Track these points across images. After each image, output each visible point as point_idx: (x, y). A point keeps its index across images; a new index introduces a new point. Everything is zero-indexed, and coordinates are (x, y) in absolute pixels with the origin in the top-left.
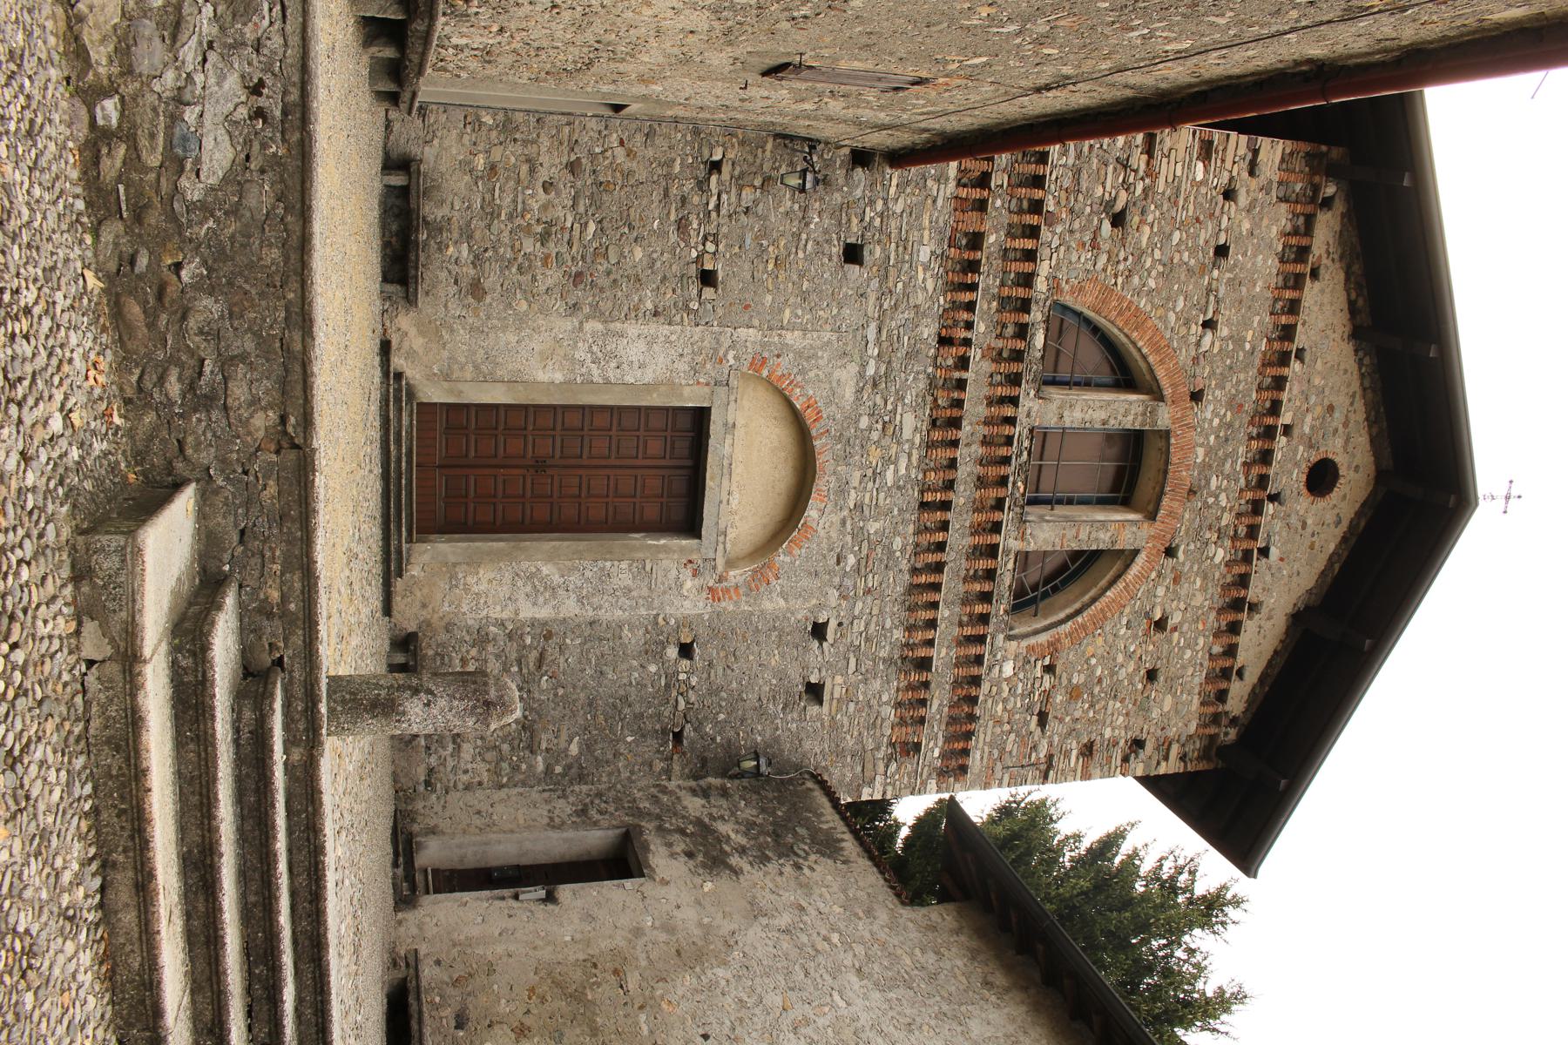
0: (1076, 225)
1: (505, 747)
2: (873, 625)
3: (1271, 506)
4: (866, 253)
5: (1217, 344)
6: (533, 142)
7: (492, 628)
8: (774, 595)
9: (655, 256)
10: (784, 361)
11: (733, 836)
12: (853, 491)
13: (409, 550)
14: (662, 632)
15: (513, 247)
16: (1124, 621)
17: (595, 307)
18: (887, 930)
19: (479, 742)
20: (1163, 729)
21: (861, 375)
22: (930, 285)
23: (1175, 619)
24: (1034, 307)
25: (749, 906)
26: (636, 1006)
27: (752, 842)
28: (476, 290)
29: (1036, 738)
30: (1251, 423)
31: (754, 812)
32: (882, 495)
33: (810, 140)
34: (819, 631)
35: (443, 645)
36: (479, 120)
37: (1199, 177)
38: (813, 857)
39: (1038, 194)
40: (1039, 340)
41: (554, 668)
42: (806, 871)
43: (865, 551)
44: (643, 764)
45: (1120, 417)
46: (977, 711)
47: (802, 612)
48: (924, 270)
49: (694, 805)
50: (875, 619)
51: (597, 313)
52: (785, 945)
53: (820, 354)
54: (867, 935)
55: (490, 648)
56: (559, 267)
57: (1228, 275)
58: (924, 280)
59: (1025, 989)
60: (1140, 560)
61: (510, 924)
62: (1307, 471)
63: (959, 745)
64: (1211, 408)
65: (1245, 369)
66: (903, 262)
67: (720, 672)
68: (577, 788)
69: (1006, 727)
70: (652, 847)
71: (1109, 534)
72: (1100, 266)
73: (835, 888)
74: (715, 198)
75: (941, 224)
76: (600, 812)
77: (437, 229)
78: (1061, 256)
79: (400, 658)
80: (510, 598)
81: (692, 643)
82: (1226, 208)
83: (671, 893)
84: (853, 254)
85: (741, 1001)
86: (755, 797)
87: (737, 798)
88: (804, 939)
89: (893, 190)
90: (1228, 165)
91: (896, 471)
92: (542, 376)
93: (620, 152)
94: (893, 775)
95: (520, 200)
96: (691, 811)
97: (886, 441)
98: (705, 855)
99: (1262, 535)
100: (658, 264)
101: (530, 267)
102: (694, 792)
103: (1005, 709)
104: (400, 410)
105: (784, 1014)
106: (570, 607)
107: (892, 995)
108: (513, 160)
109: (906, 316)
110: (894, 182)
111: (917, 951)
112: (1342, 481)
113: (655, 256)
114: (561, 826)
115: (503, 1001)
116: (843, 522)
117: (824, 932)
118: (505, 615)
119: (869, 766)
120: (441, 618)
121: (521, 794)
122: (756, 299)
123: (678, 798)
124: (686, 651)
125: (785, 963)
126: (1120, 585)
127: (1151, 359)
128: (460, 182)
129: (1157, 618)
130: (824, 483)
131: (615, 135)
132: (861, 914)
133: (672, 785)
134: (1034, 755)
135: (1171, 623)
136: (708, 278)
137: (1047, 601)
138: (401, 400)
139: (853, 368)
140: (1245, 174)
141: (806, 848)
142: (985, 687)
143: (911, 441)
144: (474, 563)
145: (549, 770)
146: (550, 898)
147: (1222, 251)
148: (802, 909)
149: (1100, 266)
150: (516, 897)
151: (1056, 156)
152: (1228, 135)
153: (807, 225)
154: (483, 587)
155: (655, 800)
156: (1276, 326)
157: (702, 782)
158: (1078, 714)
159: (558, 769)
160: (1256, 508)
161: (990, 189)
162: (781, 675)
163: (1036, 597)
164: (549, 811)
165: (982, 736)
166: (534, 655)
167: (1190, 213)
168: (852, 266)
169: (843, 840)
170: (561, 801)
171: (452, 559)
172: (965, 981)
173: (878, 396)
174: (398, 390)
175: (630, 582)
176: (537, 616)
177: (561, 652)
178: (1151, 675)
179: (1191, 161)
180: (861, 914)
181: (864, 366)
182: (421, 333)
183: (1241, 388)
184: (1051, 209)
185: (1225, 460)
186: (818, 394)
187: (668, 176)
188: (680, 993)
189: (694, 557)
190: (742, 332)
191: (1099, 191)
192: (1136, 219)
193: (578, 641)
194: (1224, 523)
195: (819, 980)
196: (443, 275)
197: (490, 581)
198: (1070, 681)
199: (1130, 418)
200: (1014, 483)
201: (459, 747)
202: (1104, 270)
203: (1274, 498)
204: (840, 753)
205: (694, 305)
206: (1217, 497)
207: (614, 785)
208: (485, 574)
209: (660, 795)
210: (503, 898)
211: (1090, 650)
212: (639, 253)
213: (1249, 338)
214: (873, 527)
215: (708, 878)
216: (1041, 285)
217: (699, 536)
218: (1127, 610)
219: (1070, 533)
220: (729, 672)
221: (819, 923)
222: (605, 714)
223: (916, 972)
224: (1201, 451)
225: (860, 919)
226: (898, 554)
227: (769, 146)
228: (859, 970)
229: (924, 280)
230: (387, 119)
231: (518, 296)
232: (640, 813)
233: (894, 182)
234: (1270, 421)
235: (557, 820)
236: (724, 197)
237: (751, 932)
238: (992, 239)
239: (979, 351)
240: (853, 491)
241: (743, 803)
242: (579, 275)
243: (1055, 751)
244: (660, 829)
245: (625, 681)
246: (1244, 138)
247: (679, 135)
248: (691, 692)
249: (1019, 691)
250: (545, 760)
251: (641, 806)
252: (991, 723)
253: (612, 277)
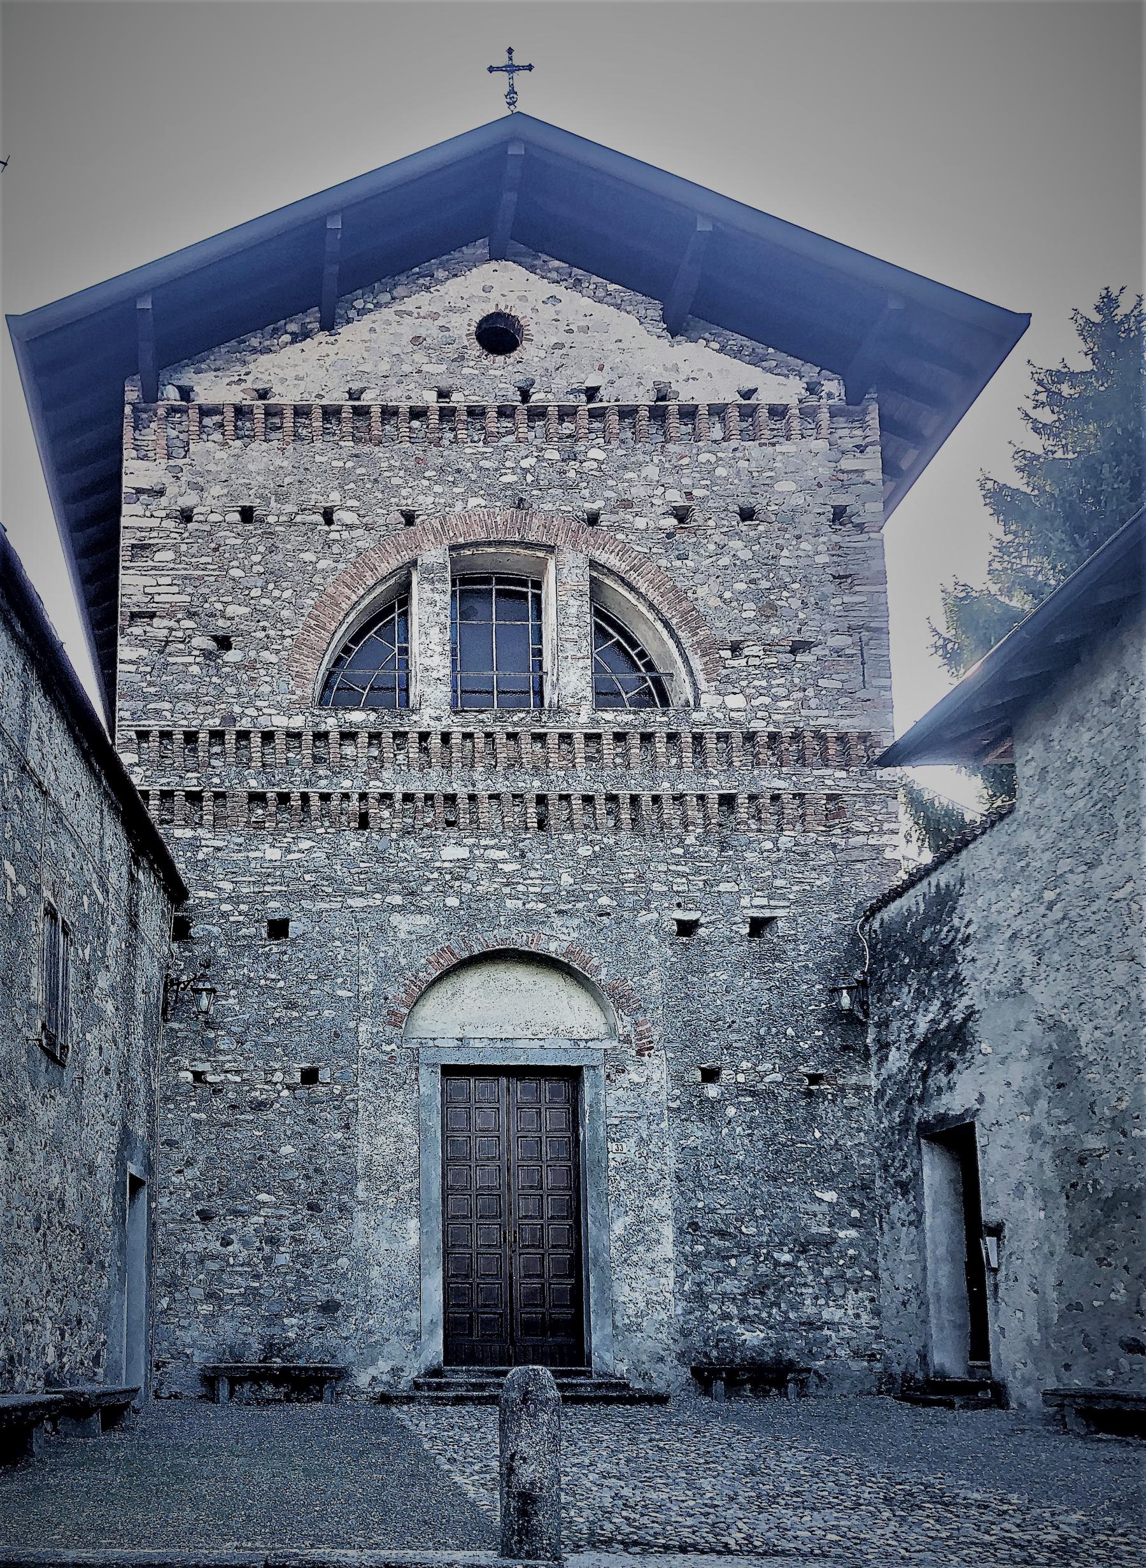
0: (232, 690)
1: (827, 1272)
2: (680, 868)
3: (534, 398)
4: (277, 917)
5: (350, 503)
6: (183, 1256)
7: (686, 1288)
8: (644, 983)
9: (289, 1133)
10: (391, 992)
11: (930, 1016)
12: (527, 906)
13: (599, 1376)
14: (689, 1102)
15: (286, 1274)
16: (678, 563)
17: (343, 1189)
18: (1042, 832)
19: (822, 1301)
20: (820, 485)
21: (401, 909)
22: (305, 844)
23: (676, 497)
24: (323, 728)
25: (1010, 1000)
26: (1123, 1140)
27: (938, 993)
28: (329, 1308)
29: (827, 652)
30: (438, 443)
31: (906, 990)
32: (533, 874)
33: (166, 985)
34: (687, 928)
35: (706, 1342)
36: (166, 1311)
37: (169, 555)
38: (956, 922)
39: (203, 736)
40: (357, 716)
41: (732, 1219)
42: (970, 930)
43: (595, 887)
44: (849, 1118)
45: (437, 609)
46: (787, 731)
47: (664, 953)
48: (290, 852)
49: (897, 1060)
50: (673, 867)
51: (348, 1189)
52: (1056, 957)
53: (382, 955)
54: (1048, 855)
55: (708, 1289)
56: (304, 1226)
57: (273, 504)
58: (301, 851)
59: (1122, 648)
60: (602, 557)
61: (1025, 1280)
62: (491, 357)
63: (833, 748)
64: (421, 498)
65: (375, 463)
66: (282, 876)
67: (734, 1036)
68: (879, 1192)
69: (810, 692)
70: (942, 1111)
71: (572, 602)
72: (274, 659)
73: (991, 895)
74: (229, 1075)
75: (241, 840)
76: (904, 1167)
77: (271, 1348)
78: (266, 704)
79: (719, 1386)
80: (652, 1269)
81: (702, 1070)
82: (202, 518)
83: (992, 1092)
84: (278, 929)
85: (1120, 1012)
86: (888, 989)
87: (889, 1010)
88: (1049, 933)
89: (211, 895)
90: (154, 523)
91: (504, 861)
92: (414, 1241)
93: (189, 1173)
94: (870, 824)
95: (239, 1269)
96: (904, 1064)
97: (472, 875)
98: (951, 1048)
99: (571, 400)
100: (297, 1128)
101: (304, 1256)
102: (883, 1059)
103: (786, 698)
104: (448, 1384)
105: (1138, 960)
106: (662, 1204)
107: (1122, 827)
108: (201, 1277)
109: (339, 867)
110: (202, 894)
111: (1070, 792)
112: (502, 307)
113: (289, 1133)
114: (919, 1213)
115: (1113, 1296)
116: (560, 912)
117: (1042, 910)
118: (672, 1274)
119: (855, 854)
120: (675, 1341)
121: (885, 1255)
122: (328, 1026)
123: (889, 1077)
124: (710, 1075)
125: (1077, 958)
126: (632, 577)
127: (371, 582)
128: (227, 1328)
129: (675, 522)
130: (519, 939)
131: (174, 1179)
132: (1023, 863)
133: (875, 1083)
134: (847, 651)
135: (681, 502)
136: (310, 1077)
137: (656, 663)
138: (438, 1384)
139: (396, 919)
140: (164, 501)
141: (945, 929)
142: (757, 725)
143: (471, 848)
144: (610, 1308)
145: (854, 1224)
146: (997, 1231)
147: (247, 515)
148: (1014, 936)
149: (274, 659)
150: (995, 1271)
151: (163, 723)
152: (125, 528)
153: (250, 979)
154: (638, 1296)
155: (892, 1103)
156: (325, 432)
157: (873, 1049)
158: (796, 603)
159: (855, 1213)
160: (537, 414)
161: (202, 791)
162: (741, 966)
163: (651, 678)
164: (903, 1225)
165: (821, 721)
166: (715, 1241)
167: (209, 560)
168: (290, 929)
169: (938, 886)
170: (892, 1211)
171: (609, 1330)
172: (1109, 729)
173: (426, 889)
174: (430, 1387)
175: (632, 1140)
176: (671, 1240)
177: (713, 1211)
178: (747, 514)
179: (154, 568)
180: (1023, 863)
181: (393, 908)
182: (374, 1362)
183: (397, 464)
184: (218, 721)
185: (481, 468)
186: (424, 953)
187: (210, 1122)
188: (1106, 1086)
189: (602, 1072)
190: (362, 1037)
191: (195, 669)
192: (221, 622)
193: (700, 1195)
194: (556, 456)
195: (1098, 917)
196: (315, 1343)
197: (633, 1289)
198: (752, 621)
199: (437, 597)
200: (515, 724)
201: (826, 1323)
202: (278, 652)
203: (525, 396)
204: (837, 892)
205: (337, 1089)
206: (526, 471)
207: (875, 1149)
208: (622, 1292)
209: (887, 1098)
210: (996, 1286)
211: (714, 602)
212: (287, 1150)
213: (341, 464)
214: (566, 880)
215: (976, 1047)
216: (297, 722)
217: (580, 1068)
218: (664, 563)
219: (570, 650)
220: (735, 1026)
221: (1030, 914)
222: (786, 1162)
223: (1094, 793)
224: (473, 502)
225: (1028, 865)
226: (597, 848)
227: (175, 1025)
228: (1091, 866)
229: (301, 851)
230: (169, 1398)
231: (334, 1266)
232: (906, 1121)
233: (202, 894)
234: (434, 418)
235: (913, 1217)
236: (227, 1066)
237: (1040, 998)
238: (253, 783)
239: (372, 783)
240: (527, 906)
241: (895, 1003)
242: (310, 1207)
243: (843, 625)
244: (922, 1100)
245: (746, 1141)
246: (126, 509)
247: (169, 1116)
248: (759, 1068)
249: (764, 683)
250: (842, 1228)
251: (897, 1120)
252: (803, 712)
253: (311, 1173)
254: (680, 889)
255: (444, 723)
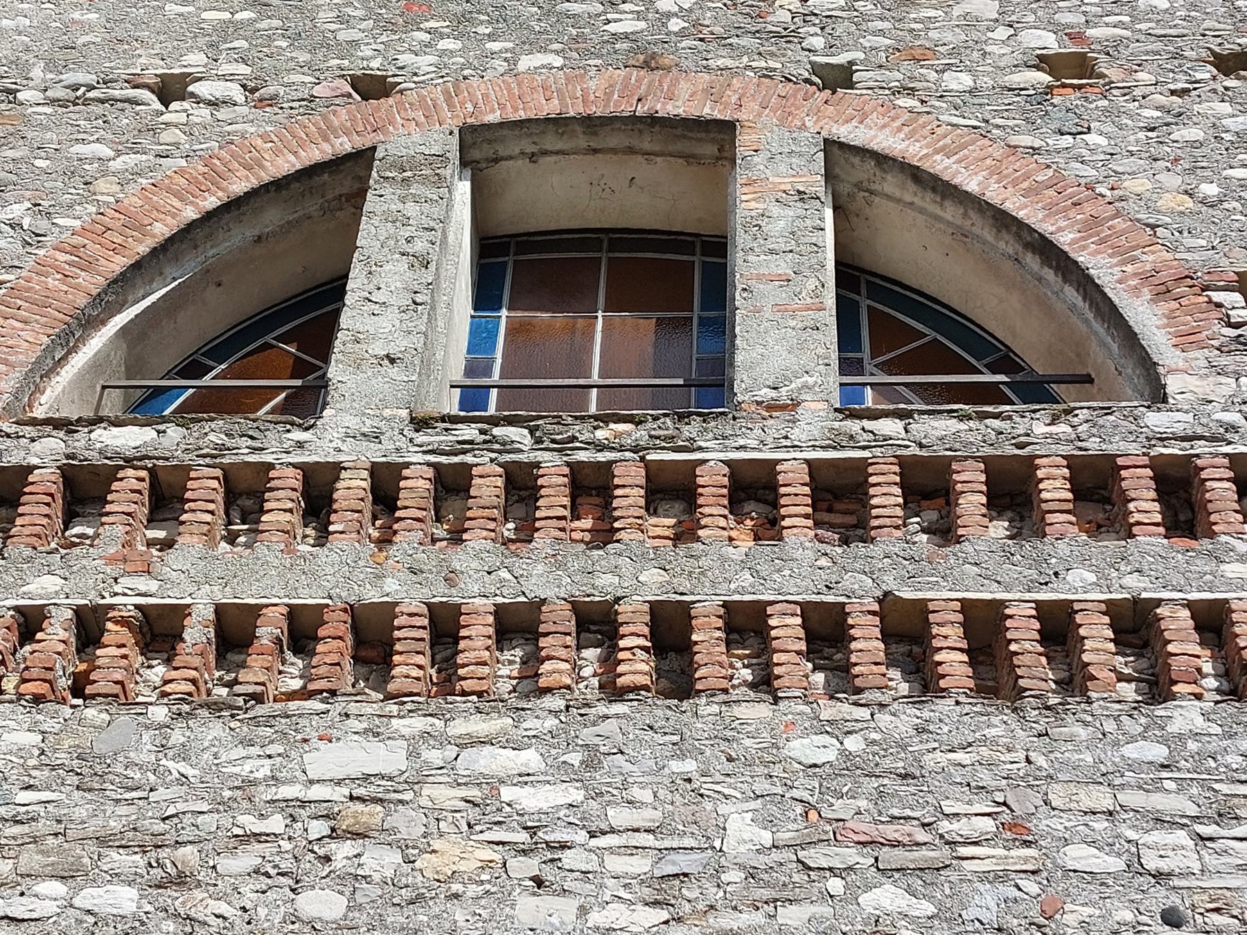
2: (1158, 802)
5: (226, 69)
32: (619, 816)
71: (775, 210)
91: (524, 778)
254: (1164, 865)
255: (388, 445)
